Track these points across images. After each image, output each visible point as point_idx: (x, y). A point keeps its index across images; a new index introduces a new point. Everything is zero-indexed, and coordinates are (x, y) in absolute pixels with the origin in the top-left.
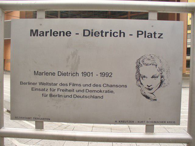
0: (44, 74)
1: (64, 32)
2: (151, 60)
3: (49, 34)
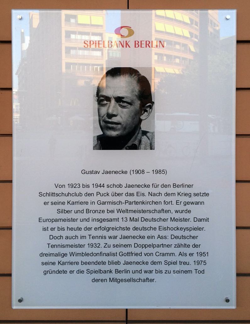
0: (134, 203)
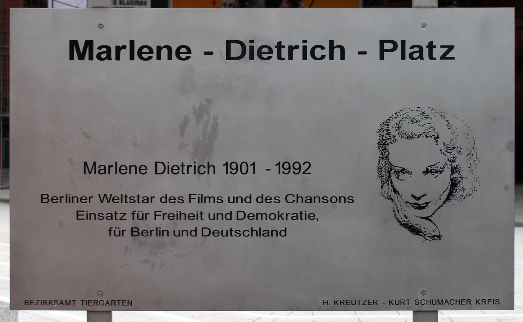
0: (113, 169)
1: (169, 48)
2: (422, 123)
3: (125, 54)
